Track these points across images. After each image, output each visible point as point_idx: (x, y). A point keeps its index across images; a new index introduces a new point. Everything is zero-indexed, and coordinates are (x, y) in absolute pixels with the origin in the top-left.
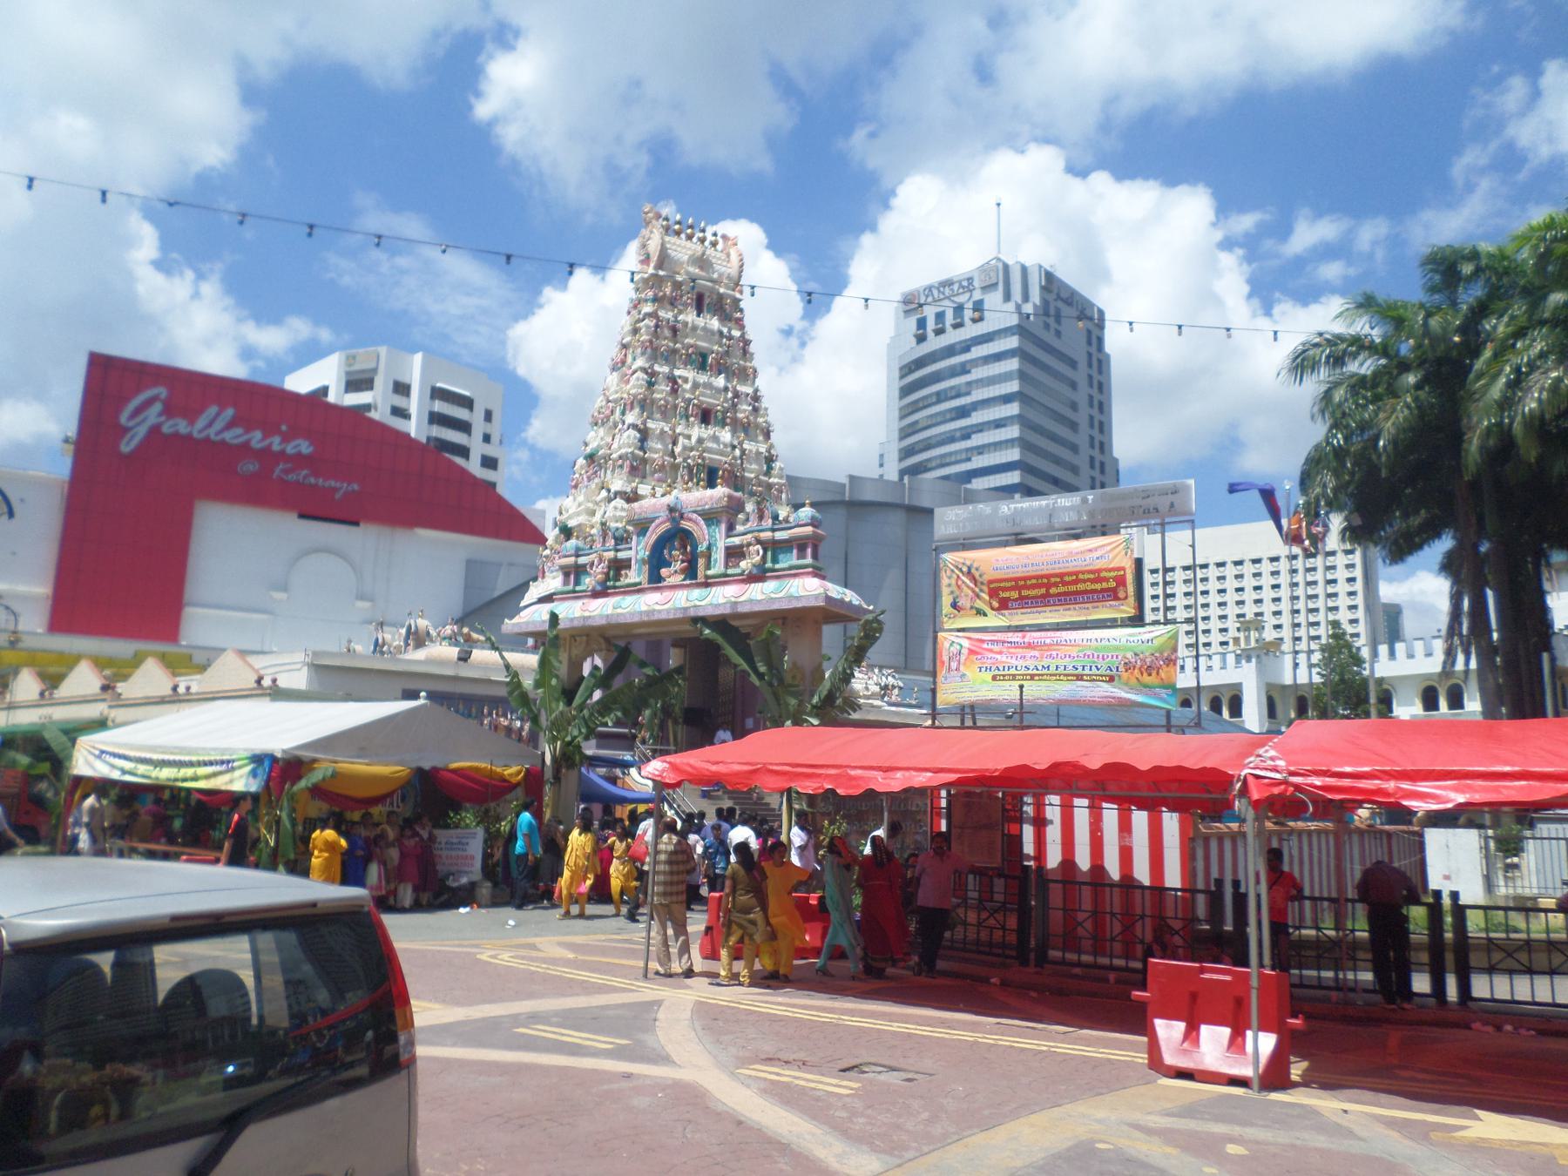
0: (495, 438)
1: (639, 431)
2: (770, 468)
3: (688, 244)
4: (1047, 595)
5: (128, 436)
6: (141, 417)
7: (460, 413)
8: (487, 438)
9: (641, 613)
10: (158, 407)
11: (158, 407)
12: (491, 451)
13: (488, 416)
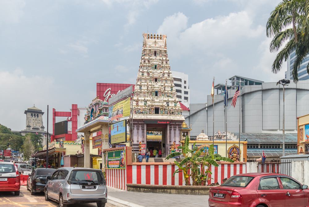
0: (187, 87)
1: (140, 86)
2: (172, 89)
3: (152, 40)
4: (170, 122)
5: (105, 98)
6: (107, 95)
7: (178, 83)
8: (185, 87)
9: (105, 120)
10: (109, 92)
11: (109, 92)
12: (186, 90)
13: (185, 82)
